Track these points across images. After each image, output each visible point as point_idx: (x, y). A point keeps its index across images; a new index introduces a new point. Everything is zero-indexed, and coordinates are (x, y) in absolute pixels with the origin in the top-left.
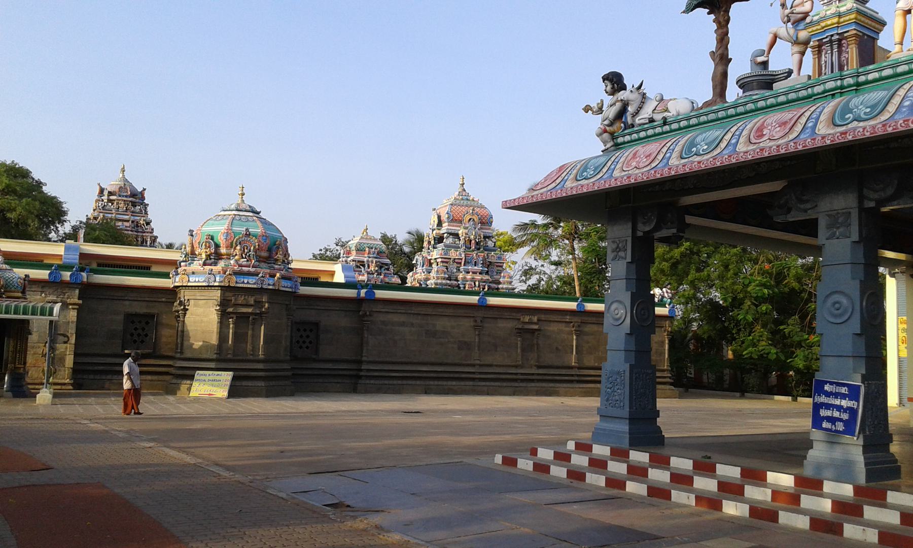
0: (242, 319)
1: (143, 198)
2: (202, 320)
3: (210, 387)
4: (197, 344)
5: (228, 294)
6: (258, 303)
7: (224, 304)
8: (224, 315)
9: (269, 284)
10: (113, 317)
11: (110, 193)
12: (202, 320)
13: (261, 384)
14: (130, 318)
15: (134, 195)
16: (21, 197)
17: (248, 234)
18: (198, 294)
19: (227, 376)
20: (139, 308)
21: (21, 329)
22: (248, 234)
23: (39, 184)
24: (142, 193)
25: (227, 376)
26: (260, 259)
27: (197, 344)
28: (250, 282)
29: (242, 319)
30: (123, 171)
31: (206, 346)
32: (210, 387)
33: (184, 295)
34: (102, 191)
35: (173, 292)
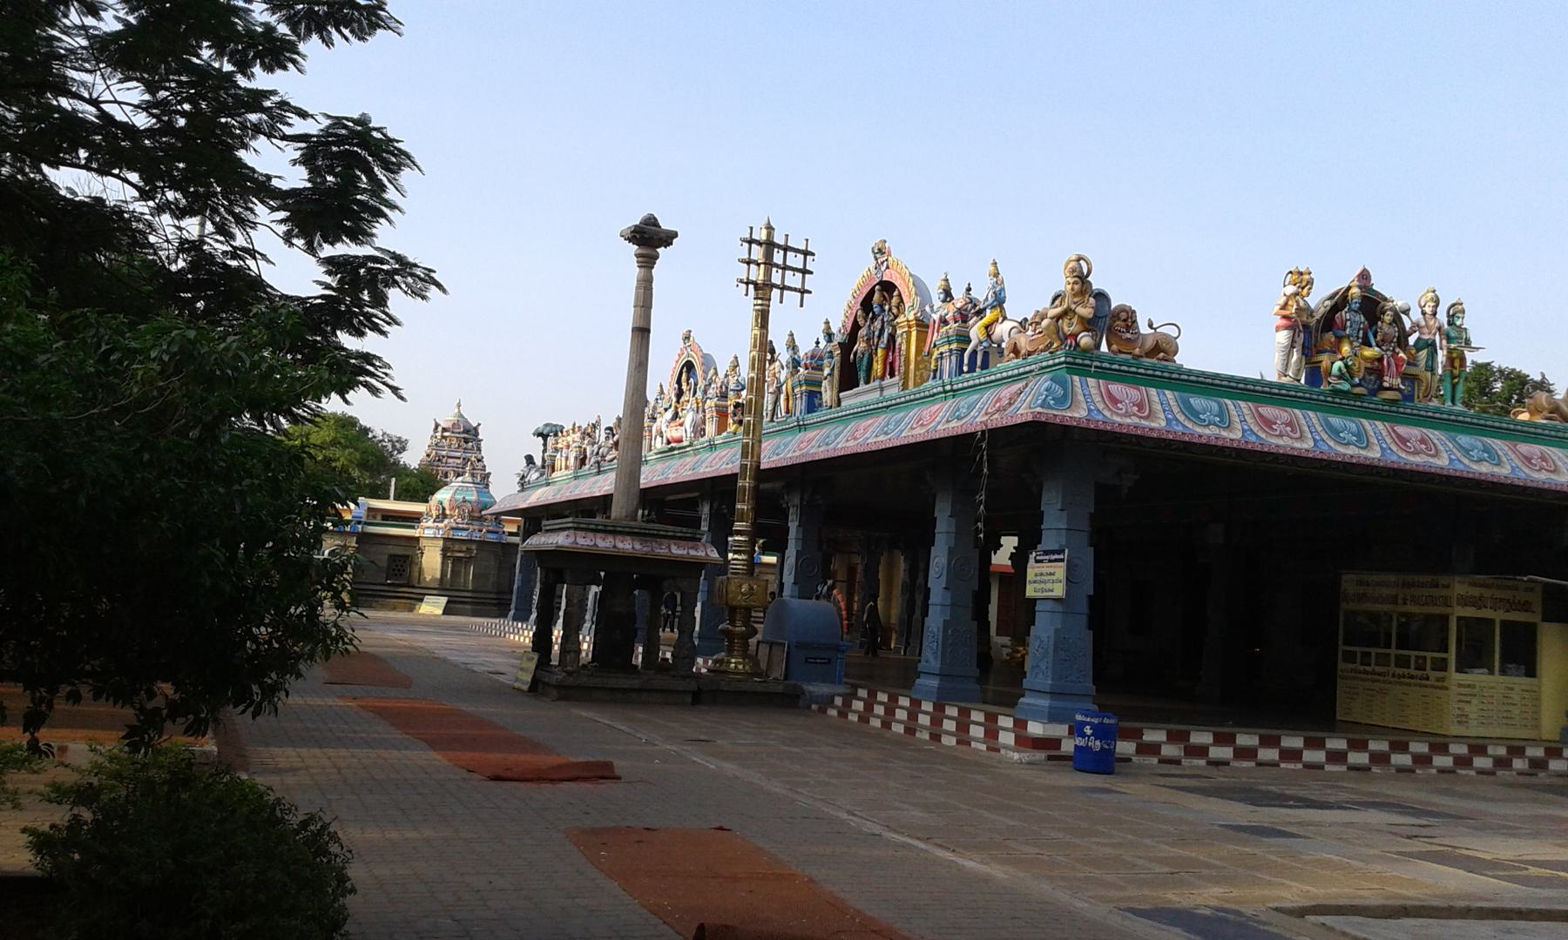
0: (456, 560)
1: (477, 434)
2: (431, 562)
3: (432, 607)
4: (428, 578)
5: (449, 544)
6: (468, 550)
7: (445, 550)
8: (444, 557)
9: (477, 536)
10: (382, 556)
11: (444, 430)
12: (431, 562)
13: (468, 607)
14: (393, 558)
15: (467, 431)
16: (345, 447)
17: (465, 501)
18: (430, 543)
19: (444, 600)
20: (399, 551)
21: (1445, 619)
22: (465, 501)
23: (366, 430)
24: (476, 429)
25: (444, 600)
26: (472, 518)
27: (428, 578)
28: (463, 535)
29: (456, 560)
30: (459, 405)
31: (433, 579)
32: (432, 607)
33: (423, 543)
34: (437, 426)
35: (417, 539)
